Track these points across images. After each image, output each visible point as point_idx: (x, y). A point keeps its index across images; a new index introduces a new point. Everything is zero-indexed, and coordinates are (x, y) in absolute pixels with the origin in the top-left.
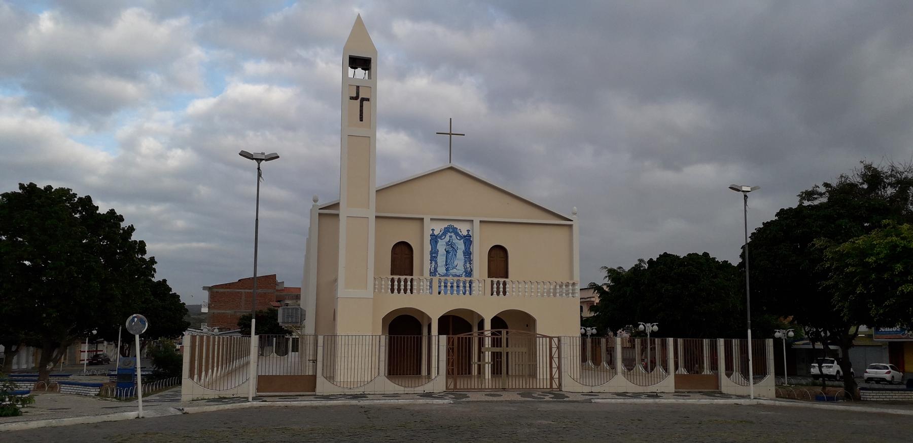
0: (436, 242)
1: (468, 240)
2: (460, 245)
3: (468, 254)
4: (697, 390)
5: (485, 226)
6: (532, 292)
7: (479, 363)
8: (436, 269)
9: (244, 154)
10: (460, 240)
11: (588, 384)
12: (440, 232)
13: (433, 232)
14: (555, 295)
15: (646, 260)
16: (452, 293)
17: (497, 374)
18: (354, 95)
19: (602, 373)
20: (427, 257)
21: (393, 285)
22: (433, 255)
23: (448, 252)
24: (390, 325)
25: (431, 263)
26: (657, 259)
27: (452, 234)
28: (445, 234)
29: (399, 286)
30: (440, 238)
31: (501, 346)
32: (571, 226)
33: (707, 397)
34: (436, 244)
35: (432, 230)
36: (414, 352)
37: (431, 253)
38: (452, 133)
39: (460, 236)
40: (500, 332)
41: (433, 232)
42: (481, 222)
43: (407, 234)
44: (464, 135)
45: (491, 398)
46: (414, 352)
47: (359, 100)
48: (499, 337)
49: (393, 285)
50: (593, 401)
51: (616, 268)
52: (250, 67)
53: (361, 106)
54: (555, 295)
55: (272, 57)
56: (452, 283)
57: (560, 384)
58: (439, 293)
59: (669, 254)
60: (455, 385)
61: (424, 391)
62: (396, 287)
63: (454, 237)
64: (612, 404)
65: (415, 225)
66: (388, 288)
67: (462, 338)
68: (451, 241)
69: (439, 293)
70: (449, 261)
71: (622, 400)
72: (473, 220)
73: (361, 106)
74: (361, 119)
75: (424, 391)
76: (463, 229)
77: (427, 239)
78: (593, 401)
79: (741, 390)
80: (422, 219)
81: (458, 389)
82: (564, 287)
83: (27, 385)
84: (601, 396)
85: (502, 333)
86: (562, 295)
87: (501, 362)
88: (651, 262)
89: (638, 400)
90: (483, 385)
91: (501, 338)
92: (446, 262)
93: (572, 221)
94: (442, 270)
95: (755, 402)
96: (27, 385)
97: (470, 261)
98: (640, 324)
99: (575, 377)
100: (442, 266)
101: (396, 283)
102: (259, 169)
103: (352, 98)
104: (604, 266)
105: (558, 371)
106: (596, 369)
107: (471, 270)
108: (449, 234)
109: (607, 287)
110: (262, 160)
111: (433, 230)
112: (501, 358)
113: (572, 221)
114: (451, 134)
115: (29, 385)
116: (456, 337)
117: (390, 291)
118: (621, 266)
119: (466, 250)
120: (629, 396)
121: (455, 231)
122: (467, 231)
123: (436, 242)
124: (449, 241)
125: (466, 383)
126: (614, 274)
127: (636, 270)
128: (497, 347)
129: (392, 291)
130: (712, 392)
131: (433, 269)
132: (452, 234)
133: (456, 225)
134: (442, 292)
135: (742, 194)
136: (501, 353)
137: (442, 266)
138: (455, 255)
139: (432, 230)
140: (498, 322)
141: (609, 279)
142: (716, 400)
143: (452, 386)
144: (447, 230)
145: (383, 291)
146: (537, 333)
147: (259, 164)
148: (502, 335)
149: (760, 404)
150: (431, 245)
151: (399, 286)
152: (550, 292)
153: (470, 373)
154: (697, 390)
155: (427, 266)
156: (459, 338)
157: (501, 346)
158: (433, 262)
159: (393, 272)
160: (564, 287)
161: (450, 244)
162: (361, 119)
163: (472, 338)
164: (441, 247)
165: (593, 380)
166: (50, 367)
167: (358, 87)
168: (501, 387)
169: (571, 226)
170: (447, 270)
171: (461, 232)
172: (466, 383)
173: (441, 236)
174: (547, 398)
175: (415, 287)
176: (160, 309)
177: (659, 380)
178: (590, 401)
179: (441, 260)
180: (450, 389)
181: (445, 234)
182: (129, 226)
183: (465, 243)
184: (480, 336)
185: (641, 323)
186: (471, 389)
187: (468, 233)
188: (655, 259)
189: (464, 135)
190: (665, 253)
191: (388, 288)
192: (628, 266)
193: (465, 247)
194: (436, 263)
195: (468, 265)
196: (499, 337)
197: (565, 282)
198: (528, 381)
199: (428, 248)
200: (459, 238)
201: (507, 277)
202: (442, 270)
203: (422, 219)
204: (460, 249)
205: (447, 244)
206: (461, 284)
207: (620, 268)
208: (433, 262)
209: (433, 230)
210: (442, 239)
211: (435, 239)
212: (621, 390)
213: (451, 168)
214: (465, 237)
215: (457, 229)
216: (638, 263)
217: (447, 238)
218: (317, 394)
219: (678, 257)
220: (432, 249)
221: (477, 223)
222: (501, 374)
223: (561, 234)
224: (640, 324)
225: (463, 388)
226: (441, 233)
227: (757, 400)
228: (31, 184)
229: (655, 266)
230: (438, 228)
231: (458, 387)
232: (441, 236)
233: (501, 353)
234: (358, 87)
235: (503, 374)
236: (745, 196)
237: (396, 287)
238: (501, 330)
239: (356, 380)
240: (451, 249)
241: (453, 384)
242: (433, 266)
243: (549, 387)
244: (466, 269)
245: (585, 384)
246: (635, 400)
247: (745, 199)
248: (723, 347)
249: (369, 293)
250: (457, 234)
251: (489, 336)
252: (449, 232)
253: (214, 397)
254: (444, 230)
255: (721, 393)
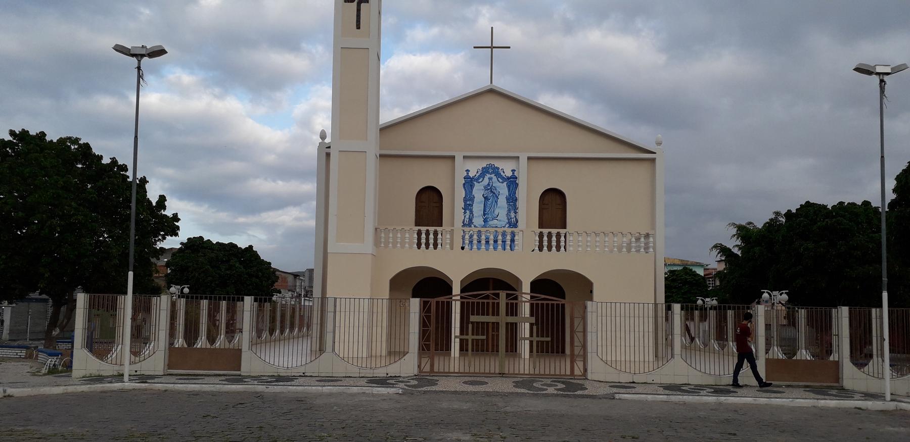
0: (472, 186)
1: (512, 182)
2: (503, 189)
3: (512, 200)
4: (801, 384)
5: (534, 164)
8: (471, 220)
9: (119, 49)
10: (502, 183)
12: (477, 173)
13: (468, 174)
15: (783, 212)
16: (479, 249)
17: (493, 351)
19: (726, 357)
20: (459, 204)
21: (419, 239)
22: (468, 203)
23: (486, 199)
25: (465, 213)
26: (797, 210)
30: (477, 180)
31: (498, 315)
32: (653, 160)
33: (812, 395)
34: (472, 189)
35: (466, 171)
37: (465, 200)
39: (503, 178)
40: (498, 295)
41: (468, 174)
42: (529, 158)
43: (434, 177)
45: (471, 388)
48: (496, 301)
49: (419, 239)
50: (617, 396)
51: (744, 224)
53: (359, 10)
54: (629, 251)
56: (471, 236)
57: (585, 370)
58: (463, 248)
59: (813, 204)
60: (432, 366)
61: (387, 374)
63: (495, 179)
65: (443, 166)
68: (491, 184)
69: (463, 248)
70: (487, 210)
71: (665, 396)
73: (359, 10)
74: (358, 27)
75: (387, 374)
76: (507, 169)
77: (460, 181)
79: (872, 386)
80: (453, 158)
82: (642, 240)
83: (17, 351)
84: (639, 389)
85: (500, 296)
86: (639, 250)
87: (498, 336)
88: (789, 214)
89: (691, 397)
90: (537, 369)
91: (498, 304)
92: (484, 211)
93: (655, 153)
94: (478, 221)
95: (891, 406)
96: (17, 351)
98: (764, 292)
99: (609, 359)
101: (423, 236)
102: (139, 68)
104: (732, 222)
105: (582, 350)
106: (721, 352)
107: (517, 221)
108: (488, 176)
109: (740, 249)
110: (143, 56)
111: (468, 171)
113: (655, 153)
114: (492, 47)
115: (20, 351)
116: (433, 301)
117: (415, 246)
118: (752, 221)
119: (510, 195)
121: (496, 171)
122: (512, 171)
123: (471, 186)
124: (489, 185)
125: (477, 363)
126: (744, 232)
127: (771, 225)
128: (483, 314)
129: (419, 245)
130: (821, 387)
131: (467, 220)
133: (497, 164)
134: (466, 247)
135: (876, 79)
136: (498, 323)
137: (479, 216)
138: (496, 202)
139: (466, 171)
140: (543, 285)
141: (738, 238)
142: (823, 401)
143: (427, 368)
144: (485, 171)
145: (399, 245)
147: (139, 61)
148: (500, 298)
149: (901, 409)
150: (465, 190)
152: (622, 247)
153: (563, 351)
154: (801, 384)
155: (460, 215)
156: (437, 303)
158: (468, 212)
159: (417, 224)
160: (642, 240)
161: (490, 188)
162: (358, 27)
164: (478, 192)
166: (57, 333)
168: (497, 371)
169: (653, 160)
170: (485, 221)
171: (504, 172)
173: (478, 178)
174: (551, 390)
175: (439, 241)
176: (246, 276)
178: (612, 397)
179: (478, 208)
180: (425, 372)
182: (141, 178)
183: (509, 187)
184: (463, 300)
185: (766, 291)
186: (449, 373)
187: (513, 173)
188: (794, 211)
189: (509, 48)
190: (808, 202)
192: (760, 220)
193: (509, 191)
194: (471, 212)
195: (513, 215)
196: (496, 301)
197: (644, 232)
198: (473, 363)
199: (460, 193)
200: (501, 180)
202: (478, 221)
203: (453, 158)
205: (486, 188)
206: (500, 237)
207: (750, 223)
208: (468, 212)
209: (468, 171)
210: (479, 182)
211: (469, 183)
212: (679, 381)
213: (492, 91)
214: (508, 178)
215: (498, 168)
216: (773, 216)
218: (242, 374)
219: (824, 207)
221: (523, 161)
222: (498, 351)
223: (641, 171)
224: (764, 292)
225: (478, 371)
226: (478, 175)
227: (896, 403)
228: (87, 144)
229: (794, 219)
230: (474, 168)
231: (436, 369)
232: (478, 178)
233: (498, 323)
235: (500, 353)
236: (882, 81)
238: (497, 292)
239: (351, 356)
240: (491, 194)
242: (467, 217)
243: (568, 372)
244: (509, 219)
245: (703, 370)
247: (881, 87)
248: (847, 319)
249: (368, 246)
250: (498, 175)
251: (458, 300)
252: (488, 172)
253: (112, 374)
254: (482, 171)
255: (842, 389)
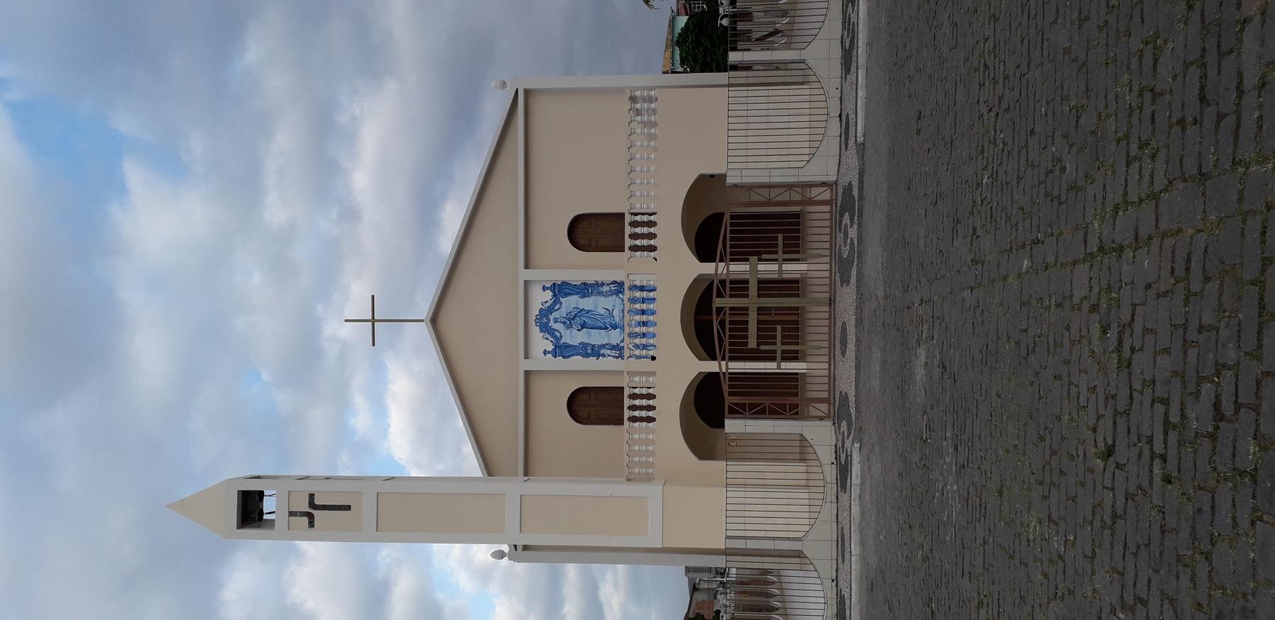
0: (567, 346)
1: (560, 290)
2: (570, 303)
3: (585, 289)
5: (533, 261)
6: (648, 195)
7: (779, 356)
8: (613, 348)
10: (561, 304)
11: (823, 124)
12: (548, 339)
13: (549, 352)
14: (654, 124)
18: (305, 520)
20: (591, 363)
21: (641, 419)
22: (590, 351)
23: (583, 326)
24: (712, 427)
25: (604, 355)
27: (551, 317)
28: (551, 332)
29: (641, 408)
30: (558, 339)
31: (747, 309)
32: (527, 92)
34: (570, 346)
35: (545, 354)
36: (757, 387)
37: (586, 355)
38: (371, 318)
39: (555, 303)
40: (719, 310)
41: (549, 352)
42: (527, 267)
43: (554, 400)
44: (373, 296)
45: (851, 346)
46: (757, 387)
47: (314, 512)
49: (641, 419)
52: (361, 421)
54: (654, 124)
55: (342, 404)
56: (637, 346)
57: (824, 184)
58: (653, 358)
60: (820, 400)
61: (833, 463)
62: (644, 414)
64: (868, 99)
65: (538, 386)
66: (647, 427)
67: (730, 387)
69: (653, 358)
70: (599, 324)
71: (860, 71)
72: (525, 281)
74: (348, 508)
75: (833, 463)
76: (541, 298)
77: (560, 363)
78: (860, 140)
80: (527, 373)
81: (829, 395)
82: (638, 106)
87: (776, 309)
91: (731, 309)
93: (517, 90)
94: (614, 337)
97: (598, 285)
99: (806, 151)
100: (608, 336)
103: (311, 524)
107: (614, 282)
108: (552, 323)
111: (545, 352)
112: (769, 309)
113: (517, 90)
114: (373, 321)
116: (729, 400)
119: (578, 293)
120: (852, 42)
121: (545, 313)
123: (566, 347)
124: (564, 323)
125: (816, 231)
128: (746, 330)
131: (613, 353)
132: (551, 319)
133: (535, 311)
134: (651, 353)
136: (759, 309)
137: (608, 336)
138: (588, 312)
139: (545, 354)
143: (824, 407)
144: (545, 328)
145: (651, 448)
146: (714, 272)
151: (641, 408)
155: (608, 363)
156: (731, 394)
157: (747, 309)
158: (602, 352)
160: (638, 106)
161: (569, 321)
162: (348, 508)
163: (730, 374)
164: (574, 337)
165: (810, 593)
167: (291, 514)
168: (827, 309)
170: (615, 327)
171: (546, 302)
172: (816, 231)
173: (556, 338)
177: (814, 79)
178: (861, 148)
179: (597, 338)
181: (551, 332)
183: (567, 295)
187: (548, 288)
189: (373, 296)
191: (647, 427)
193: (572, 294)
194: (603, 346)
195: (606, 289)
196: (728, 312)
197: (628, 104)
199: (577, 362)
200: (558, 306)
201: (621, 216)
202: (614, 337)
203: (527, 373)
204: (577, 304)
205: (569, 327)
206: (638, 306)
208: (602, 352)
209: (545, 352)
210: (561, 336)
211: (562, 350)
213: (434, 320)
214: (555, 295)
215: (541, 309)
217: (559, 326)
220: (579, 355)
223: (539, 105)
230: (541, 343)
231: (825, 395)
232: (556, 338)
233: (759, 309)
234: (291, 514)
237: (644, 414)
240: (578, 320)
241: (818, 405)
242: (609, 352)
243: (827, 208)
244: (612, 293)
245: (822, 18)
246: (860, 44)
249: (652, 492)
250: (551, 310)
252: (547, 324)
254: (544, 332)
